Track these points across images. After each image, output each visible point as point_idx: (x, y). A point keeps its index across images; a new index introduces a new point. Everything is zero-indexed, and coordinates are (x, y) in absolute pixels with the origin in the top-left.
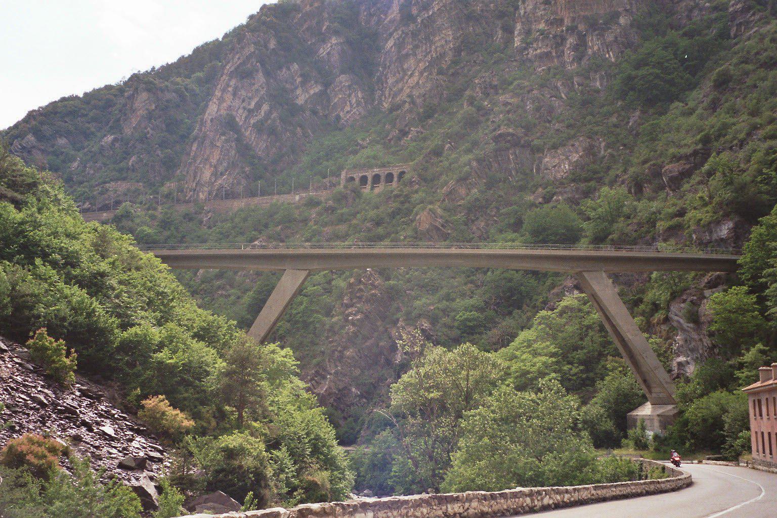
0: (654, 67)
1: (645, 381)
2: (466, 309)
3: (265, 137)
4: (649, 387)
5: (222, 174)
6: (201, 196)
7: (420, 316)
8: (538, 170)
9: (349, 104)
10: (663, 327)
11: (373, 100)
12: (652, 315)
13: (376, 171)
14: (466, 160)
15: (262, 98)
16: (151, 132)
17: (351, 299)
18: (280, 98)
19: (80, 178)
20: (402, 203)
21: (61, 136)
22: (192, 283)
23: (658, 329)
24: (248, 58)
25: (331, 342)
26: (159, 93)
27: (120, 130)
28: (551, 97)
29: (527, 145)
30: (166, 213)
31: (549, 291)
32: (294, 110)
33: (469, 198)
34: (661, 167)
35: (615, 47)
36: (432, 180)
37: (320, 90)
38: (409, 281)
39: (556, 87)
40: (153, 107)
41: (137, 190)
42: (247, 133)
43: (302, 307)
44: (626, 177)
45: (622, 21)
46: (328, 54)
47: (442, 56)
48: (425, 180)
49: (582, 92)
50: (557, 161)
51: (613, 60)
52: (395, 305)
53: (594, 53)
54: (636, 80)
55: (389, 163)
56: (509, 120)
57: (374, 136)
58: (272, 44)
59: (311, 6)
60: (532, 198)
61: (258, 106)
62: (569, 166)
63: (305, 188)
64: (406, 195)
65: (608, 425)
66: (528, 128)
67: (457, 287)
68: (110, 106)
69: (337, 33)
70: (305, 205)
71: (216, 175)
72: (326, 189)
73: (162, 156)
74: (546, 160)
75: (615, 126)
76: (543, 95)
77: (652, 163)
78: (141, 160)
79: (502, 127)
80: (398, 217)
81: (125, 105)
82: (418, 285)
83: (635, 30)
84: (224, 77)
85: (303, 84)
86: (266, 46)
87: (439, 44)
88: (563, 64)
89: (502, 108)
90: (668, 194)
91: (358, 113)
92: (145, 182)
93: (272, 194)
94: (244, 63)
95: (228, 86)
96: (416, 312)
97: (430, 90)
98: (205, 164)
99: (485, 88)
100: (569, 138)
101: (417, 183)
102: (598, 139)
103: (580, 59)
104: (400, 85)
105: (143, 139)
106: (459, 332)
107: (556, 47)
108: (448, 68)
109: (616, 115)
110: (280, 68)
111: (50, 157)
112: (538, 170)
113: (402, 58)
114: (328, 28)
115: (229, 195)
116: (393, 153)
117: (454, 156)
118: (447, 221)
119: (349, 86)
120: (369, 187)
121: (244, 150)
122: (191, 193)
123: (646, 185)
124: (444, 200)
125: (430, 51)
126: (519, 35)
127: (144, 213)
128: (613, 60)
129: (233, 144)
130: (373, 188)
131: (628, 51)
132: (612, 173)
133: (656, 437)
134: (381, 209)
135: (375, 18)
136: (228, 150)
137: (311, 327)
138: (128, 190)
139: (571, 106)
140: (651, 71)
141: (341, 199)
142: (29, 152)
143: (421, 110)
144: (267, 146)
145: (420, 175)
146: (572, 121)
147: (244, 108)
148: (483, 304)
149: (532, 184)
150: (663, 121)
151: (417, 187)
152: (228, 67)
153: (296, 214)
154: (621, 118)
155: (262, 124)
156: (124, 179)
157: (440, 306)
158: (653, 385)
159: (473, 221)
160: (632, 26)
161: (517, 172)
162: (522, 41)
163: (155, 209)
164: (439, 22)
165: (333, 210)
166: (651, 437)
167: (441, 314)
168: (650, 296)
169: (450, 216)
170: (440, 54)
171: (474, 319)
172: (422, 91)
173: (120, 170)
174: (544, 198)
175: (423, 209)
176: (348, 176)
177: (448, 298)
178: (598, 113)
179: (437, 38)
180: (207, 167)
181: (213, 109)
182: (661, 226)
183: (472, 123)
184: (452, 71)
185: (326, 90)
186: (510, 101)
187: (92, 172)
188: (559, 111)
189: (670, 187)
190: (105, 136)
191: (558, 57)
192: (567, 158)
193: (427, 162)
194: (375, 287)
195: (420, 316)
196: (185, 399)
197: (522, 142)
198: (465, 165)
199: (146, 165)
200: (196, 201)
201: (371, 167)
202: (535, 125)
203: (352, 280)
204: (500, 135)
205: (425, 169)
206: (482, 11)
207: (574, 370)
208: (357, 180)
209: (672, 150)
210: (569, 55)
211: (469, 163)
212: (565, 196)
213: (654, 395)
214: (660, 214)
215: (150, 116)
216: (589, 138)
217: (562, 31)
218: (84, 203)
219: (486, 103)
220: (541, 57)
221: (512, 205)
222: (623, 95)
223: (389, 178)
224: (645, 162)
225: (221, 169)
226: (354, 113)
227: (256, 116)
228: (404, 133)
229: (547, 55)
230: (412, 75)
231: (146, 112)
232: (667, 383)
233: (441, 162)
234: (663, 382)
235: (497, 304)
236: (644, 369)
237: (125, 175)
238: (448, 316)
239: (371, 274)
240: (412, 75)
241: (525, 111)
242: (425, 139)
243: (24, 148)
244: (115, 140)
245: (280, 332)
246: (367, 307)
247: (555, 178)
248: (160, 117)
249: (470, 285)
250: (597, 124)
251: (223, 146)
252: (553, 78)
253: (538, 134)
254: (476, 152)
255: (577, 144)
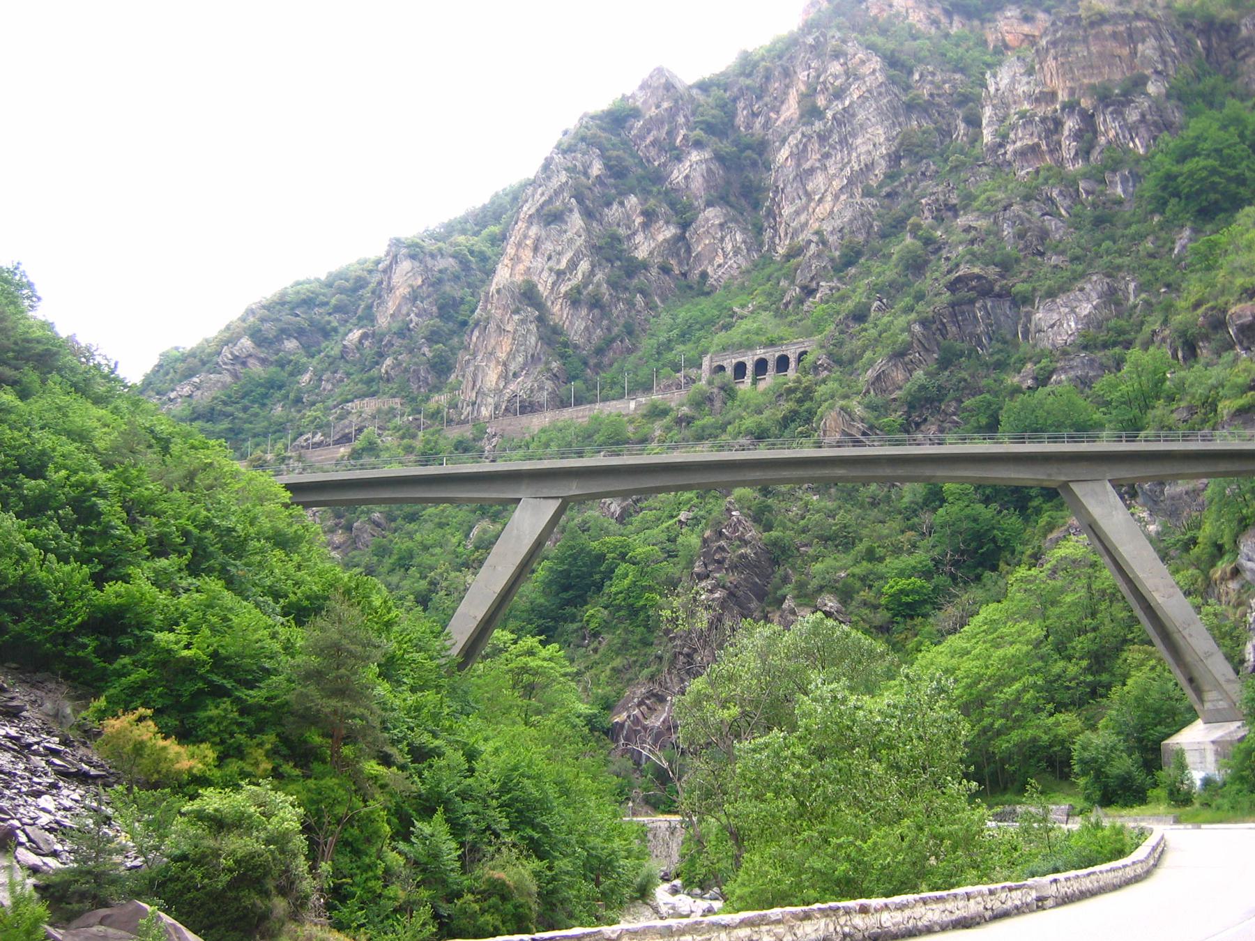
0: (1208, 156)
1: (1191, 680)
2: (901, 574)
3: (584, 312)
4: (1199, 692)
5: (515, 375)
6: (485, 412)
7: (821, 589)
8: (1025, 336)
9: (722, 250)
10: (1233, 585)
11: (761, 245)
12: (1213, 565)
13: (760, 353)
14: (898, 323)
15: (577, 254)
16: (415, 319)
17: (706, 565)
18: (609, 250)
19: (313, 398)
20: (800, 401)
21: (289, 336)
22: (460, 549)
23: (1223, 588)
24: (557, 193)
25: (671, 639)
26: (428, 259)
27: (372, 321)
28: (1043, 215)
29: (1004, 294)
30: (428, 442)
31: (1045, 536)
32: (633, 268)
33: (908, 385)
34: (1225, 311)
35: (1142, 131)
36: (851, 362)
37: (675, 235)
38: (804, 530)
39: (1050, 199)
40: (419, 282)
41: (392, 409)
42: (556, 309)
43: (626, 582)
44: (1167, 332)
45: (1151, 89)
46: (687, 177)
47: (869, 167)
48: (839, 362)
49: (1094, 205)
50: (1056, 317)
51: (1141, 151)
52: (780, 572)
53: (1109, 142)
54: (1180, 179)
55: (781, 339)
56: (973, 254)
57: (761, 299)
58: (597, 168)
59: (658, 107)
60: (1016, 379)
61: (573, 265)
62: (1076, 324)
63: (647, 388)
64: (806, 388)
65: (1124, 764)
66: (1006, 266)
67: (887, 537)
68: (362, 287)
69: (698, 144)
70: (644, 416)
71: (505, 377)
72: (679, 387)
73: (430, 355)
74: (1039, 315)
75: (1152, 256)
76: (1029, 212)
77: (1209, 305)
78: (400, 364)
79: (962, 267)
80: (793, 425)
81: (380, 283)
82: (820, 537)
83: (1173, 102)
84: (520, 223)
85: (646, 226)
86: (586, 174)
87: (863, 149)
88: (1060, 163)
89: (963, 236)
90: (1237, 357)
91: (735, 266)
92: (403, 397)
93: (593, 402)
94: (550, 201)
95: (525, 237)
96: (814, 584)
97: (851, 222)
98: (489, 360)
99: (938, 210)
100: (1075, 279)
101: (826, 369)
102: (1124, 278)
103: (1088, 153)
104: (803, 218)
105: (404, 332)
106: (889, 615)
107: (1047, 137)
108: (880, 186)
109: (1151, 238)
110: (609, 204)
111: (273, 369)
112: (1026, 333)
113: (804, 176)
114: (685, 137)
115: (525, 407)
116: (790, 324)
117: (886, 319)
118: (871, 427)
119: (721, 225)
120: (748, 379)
121: (551, 335)
122: (470, 408)
123: (1201, 344)
124: (868, 391)
125: (849, 161)
126: (989, 125)
127: (396, 443)
128: (1141, 151)
129: (533, 327)
130: (755, 382)
131: (1166, 136)
132: (1147, 329)
133: (1207, 782)
134: (767, 413)
135: (761, 120)
136: (524, 336)
137: (642, 616)
138: (379, 411)
139: (1076, 229)
140: (1202, 163)
141: (702, 402)
142: (244, 364)
143: (837, 253)
144: (587, 328)
145: (830, 355)
146: (1078, 251)
147: (551, 270)
148: (931, 564)
149: (1016, 356)
150: (1222, 238)
151: (826, 373)
152: (525, 209)
153: (630, 431)
154: (1160, 243)
155: (579, 293)
156: (373, 395)
157: (857, 570)
158: (1206, 688)
159: (918, 425)
160: (1168, 96)
161: (991, 339)
162: (996, 133)
163: (414, 436)
164: (861, 115)
165: (688, 420)
166: (1198, 783)
167: (858, 584)
168: (1206, 532)
169: (877, 418)
170: (866, 165)
171: (913, 591)
172: (838, 223)
173: (370, 381)
174: (1035, 379)
175: (831, 407)
176: (715, 364)
177: (870, 556)
178: (1123, 236)
179: (859, 141)
180: (492, 365)
181: (503, 275)
182: (1226, 407)
183: (916, 266)
184: (886, 189)
185: (684, 232)
186: (974, 224)
187: (329, 387)
188: (1057, 237)
189: (1241, 343)
190: (350, 330)
191: (1051, 152)
192: (1073, 311)
193: (842, 332)
194: (746, 543)
195: (821, 589)
196: (211, 720)
197: (997, 288)
198: (903, 330)
199: (406, 370)
200: (476, 420)
201: (750, 347)
202: (1017, 261)
203: (707, 533)
204: (959, 279)
205: (840, 344)
206: (931, 95)
207: (1072, 670)
208: (729, 371)
209: (1239, 281)
210: (1069, 147)
211: (908, 329)
212: (1072, 374)
213: (1208, 705)
214: (1223, 387)
215: (414, 297)
216: (1109, 276)
217: (1056, 111)
218: (314, 434)
219: (939, 233)
220: (1023, 154)
221: (981, 393)
222: (1161, 206)
223: (783, 363)
224: (1197, 305)
225: (513, 367)
226: (730, 267)
227: (569, 279)
228: (809, 292)
229: (1034, 149)
230: (820, 200)
231: (409, 290)
232: (1228, 681)
233: (866, 330)
234: (1222, 680)
235: (955, 564)
236: (1188, 659)
237: (375, 388)
238: (870, 587)
239: (739, 521)
240: (820, 200)
241: (1001, 239)
242: (843, 299)
243: (236, 358)
244: (364, 336)
245: (592, 626)
246: (733, 578)
247: (1053, 345)
248: (429, 296)
249: (909, 534)
250: (1120, 253)
251: (516, 331)
252: (1043, 184)
253: (1024, 275)
254: (919, 307)
255: (1088, 287)
